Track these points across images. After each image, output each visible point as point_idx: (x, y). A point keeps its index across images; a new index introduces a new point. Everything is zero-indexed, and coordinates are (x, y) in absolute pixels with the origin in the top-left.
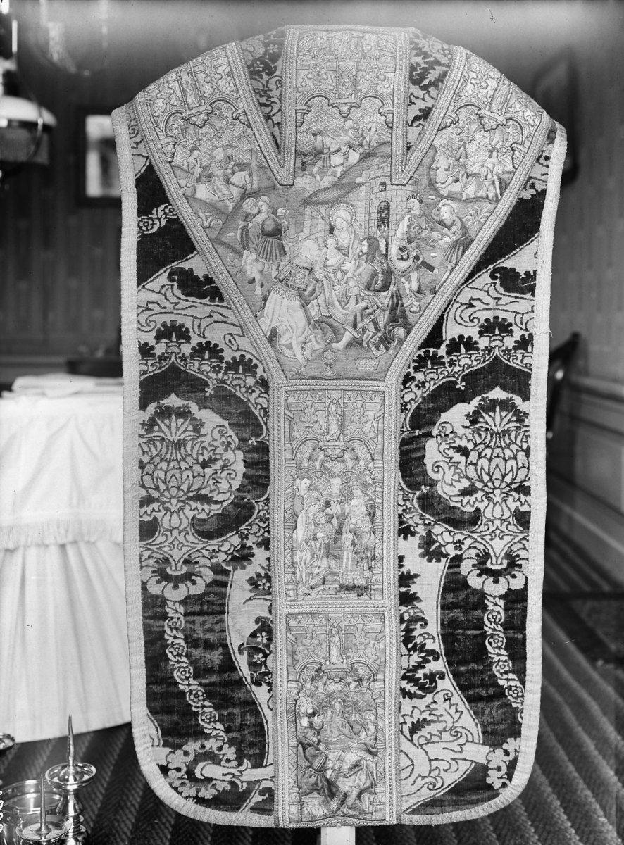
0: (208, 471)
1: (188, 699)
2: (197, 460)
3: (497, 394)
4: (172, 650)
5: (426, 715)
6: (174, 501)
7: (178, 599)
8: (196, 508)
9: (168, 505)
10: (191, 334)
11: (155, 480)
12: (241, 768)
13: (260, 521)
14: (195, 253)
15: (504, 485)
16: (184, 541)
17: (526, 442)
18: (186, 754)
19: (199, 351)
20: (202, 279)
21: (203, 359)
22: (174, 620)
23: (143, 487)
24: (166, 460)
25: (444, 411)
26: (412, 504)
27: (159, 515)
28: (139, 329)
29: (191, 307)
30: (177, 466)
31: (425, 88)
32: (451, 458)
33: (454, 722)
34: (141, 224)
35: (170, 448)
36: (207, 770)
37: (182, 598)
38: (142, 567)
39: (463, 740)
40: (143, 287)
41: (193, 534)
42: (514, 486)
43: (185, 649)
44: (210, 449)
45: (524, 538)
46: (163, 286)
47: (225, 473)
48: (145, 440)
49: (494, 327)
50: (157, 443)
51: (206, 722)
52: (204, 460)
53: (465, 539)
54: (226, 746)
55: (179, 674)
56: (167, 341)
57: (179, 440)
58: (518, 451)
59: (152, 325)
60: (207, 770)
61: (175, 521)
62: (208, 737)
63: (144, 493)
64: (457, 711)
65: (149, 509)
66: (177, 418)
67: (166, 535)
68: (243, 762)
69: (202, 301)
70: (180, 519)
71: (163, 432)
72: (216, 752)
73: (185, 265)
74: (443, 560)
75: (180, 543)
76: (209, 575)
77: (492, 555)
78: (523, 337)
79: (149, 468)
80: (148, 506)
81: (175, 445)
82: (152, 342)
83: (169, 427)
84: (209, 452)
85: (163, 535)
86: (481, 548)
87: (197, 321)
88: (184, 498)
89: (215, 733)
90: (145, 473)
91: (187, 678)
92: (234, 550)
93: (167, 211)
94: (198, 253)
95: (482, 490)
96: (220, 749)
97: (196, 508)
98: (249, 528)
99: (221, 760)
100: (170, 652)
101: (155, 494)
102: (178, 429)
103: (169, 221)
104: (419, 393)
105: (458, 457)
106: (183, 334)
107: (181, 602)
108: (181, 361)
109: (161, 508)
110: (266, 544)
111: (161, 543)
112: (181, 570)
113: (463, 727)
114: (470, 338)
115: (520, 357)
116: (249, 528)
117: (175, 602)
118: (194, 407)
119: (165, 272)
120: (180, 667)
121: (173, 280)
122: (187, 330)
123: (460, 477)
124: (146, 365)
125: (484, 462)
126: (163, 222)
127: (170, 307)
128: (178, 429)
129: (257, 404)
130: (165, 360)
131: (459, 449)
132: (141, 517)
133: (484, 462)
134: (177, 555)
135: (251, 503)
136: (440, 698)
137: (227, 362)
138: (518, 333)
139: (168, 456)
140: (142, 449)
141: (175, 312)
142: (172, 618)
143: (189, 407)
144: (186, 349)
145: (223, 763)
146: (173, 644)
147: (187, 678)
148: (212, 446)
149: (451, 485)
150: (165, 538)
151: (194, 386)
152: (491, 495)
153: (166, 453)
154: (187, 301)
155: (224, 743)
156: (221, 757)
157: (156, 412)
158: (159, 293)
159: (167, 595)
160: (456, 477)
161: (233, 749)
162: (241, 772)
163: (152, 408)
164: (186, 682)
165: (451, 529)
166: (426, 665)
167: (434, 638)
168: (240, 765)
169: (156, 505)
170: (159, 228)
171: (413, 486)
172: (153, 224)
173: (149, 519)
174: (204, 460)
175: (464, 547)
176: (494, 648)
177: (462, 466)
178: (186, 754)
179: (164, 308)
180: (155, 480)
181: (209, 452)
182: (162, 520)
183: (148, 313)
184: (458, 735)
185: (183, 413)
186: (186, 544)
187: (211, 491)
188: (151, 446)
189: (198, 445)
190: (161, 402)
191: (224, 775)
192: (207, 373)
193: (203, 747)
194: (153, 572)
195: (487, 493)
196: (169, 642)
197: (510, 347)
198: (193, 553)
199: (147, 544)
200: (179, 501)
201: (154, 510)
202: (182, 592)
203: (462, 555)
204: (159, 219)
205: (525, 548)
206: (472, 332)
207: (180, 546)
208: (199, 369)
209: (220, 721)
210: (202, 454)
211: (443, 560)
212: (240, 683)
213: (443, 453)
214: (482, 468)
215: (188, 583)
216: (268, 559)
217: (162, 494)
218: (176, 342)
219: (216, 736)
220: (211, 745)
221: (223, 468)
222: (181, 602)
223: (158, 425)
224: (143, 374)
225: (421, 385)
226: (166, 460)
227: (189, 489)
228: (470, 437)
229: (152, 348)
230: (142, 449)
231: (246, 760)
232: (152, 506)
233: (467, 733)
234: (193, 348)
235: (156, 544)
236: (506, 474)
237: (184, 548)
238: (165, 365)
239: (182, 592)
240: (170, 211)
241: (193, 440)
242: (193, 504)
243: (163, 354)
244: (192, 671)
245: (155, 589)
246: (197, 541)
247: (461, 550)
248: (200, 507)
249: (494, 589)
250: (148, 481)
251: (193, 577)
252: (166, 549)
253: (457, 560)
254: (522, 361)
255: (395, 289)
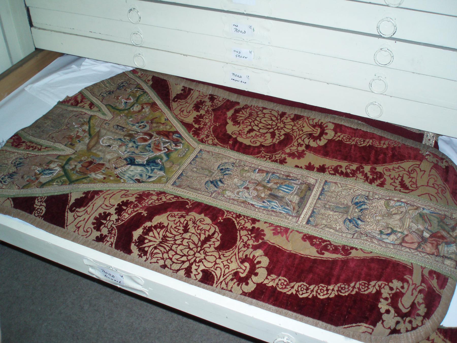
0: (192, 230)
1: (343, 295)
2: (180, 234)
3: (230, 113)
4: (301, 293)
5: (397, 182)
6: (198, 255)
7: (266, 275)
8: (210, 245)
9: (198, 260)
10: (108, 211)
11: (178, 262)
12: (410, 282)
13: (239, 218)
14: (69, 195)
15: (276, 121)
16: (226, 259)
17: (259, 108)
18: (388, 312)
19: (119, 210)
20: (84, 195)
21: (125, 210)
22: (279, 283)
23: (178, 270)
24: (169, 250)
25: (227, 131)
26: (267, 155)
27: (202, 267)
28: (87, 237)
29: (93, 205)
30: (177, 246)
31: (82, 102)
32: (252, 136)
33: (405, 171)
34: (36, 215)
35: (162, 245)
36: (405, 303)
37: (266, 273)
38: (231, 291)
39: (418, 170)
40: (67, 226)
41: (226, 252)
42: (279, 118)
43: (305, 284)
44: (178, 224)
45: (308, 118)
46: (74, 216)
47: (198, 223)
48: (150, 258)
49: (197, 107)
50: (155, 251)
51: (367, 290)
52: (183, 230)
53: (298, 142)
54: (390, 284)
55: (322, 294)
56: (103, 226)
57: (162, 239)
58: (262, 112)
59: (89, 230)
60: (405, 303)
61: (212, 259)
62: (379, 293)
63: (182, 272)
64: (398, 168)
65: (194, 272)
66: (148, 235)
67: (217, 267)
68: (406, 279)
69: (94, 199)
70: (211, 255)
71: (150, 246)
72: (393, 292)
73: (72, 201)
74: (305, 152)
75: (227, 260)
76: (259, 252)
77: (311, 132)
78: (209, 98)
79: (168, 262)
80: (192, 272)
81: (163, 241)
82: (98, 234)
83: (150, 241)
84: (180, 226)
85: (216, 269)
86: (305, 136)
87: (103, 206)
88: (199, 249)
89: (377, 287)
90: (169, 266)
91: (327, 290)
92: (250, 235)
93: (40, 200)
94: (71, 193)
95: (275, 130)
96: (391, 289)
97: (210, 245)
98: (240, 224)
99: (401, 291)
100: (302, 295)
101: (186, 265)
102: (155, 237)
103: (45, 202)
104: (210, 137)
105: (253, 134)
106: (106, 216)
107: (269, 274)
108: (118, 222)
109: (197, 264)
110: (254, 221)
111: (221, 273)
112: (246, 267)
113: (409, 168)
114: (197, 116)
115: (218, 102)
116: (240, 224)
117: (267, 278)
118: (148, 224)
119: (68, 213)
120: (317, 292)
121: (75, 210)
122: (105, 213)
123: (263, 136)
124: (108, 242)
125: (260, 125)
126: (44, 204)
127: (87, 217)
128: (155, 237)
129: (169, 199)
130: (112, 230)
131: (249, 131)
132: (197, 279)
133: (260, 125)
134: (234, 266)
135: (225, 219)
136: (387, 173)
137: (136, 201)
138: (207, 99)
139: (168, 249)
140: (154, 263)
141: (91, 214)
142: (277, 284)
143: (146, 226)
144: (114, 217)
145: (403, 291)
146: (297, 291)
147: (327, 290)
148: (177, 223)
149: (266, 140)
150: (218, 269)
151: (137, 221)
152: (279, 128)
153: (165, 248)
154: (89, 206)
155: (388, 285)
156: (398, 290)
157: (137, 246)
158: (75, 219)
159: (260, 282)
160: (263, 137)
161: (395, 281)
162: (413, 284)
163: (133, 247)
164: (330, 292)
165: (290, 146)
166: (365, 172)
167: (350, 165)
168: (408, 282)
169: (194, 267)
170: (45, 208)
171: (259, 152)
172: (41, 209)
173: (201, 274)
174: (183, 230)
175: (302, 143)
176: (364, 143)
177: (258, 134)
178: (388, 312)
179: (84, 219)
180: (178, 262)
181: (180, 226)
182: (205, 267)
183: (81, 229)
184: (414, 170)
185: (148, 231)
186: (230, 258)
187: (205, 234)
188: (155, 256)
189: (171, 229)
190: (134, 241)
191: (412, 294)
192: (134, 211)
193: (386, 299)
194: (238, 285)
195: (278, 129)
196: (294, 293)
197: (211, 104)
198: (239, 256)
199: (217, 282)
200: (199, 252)
201: (196, 270)
202: (262, 272)
203: (306, 145)
204: (41, 205)
205: (313, 119)
206: (195, 114)
207: (229, 261)
208: (129, 214)
209: (369, 281)
210: (179, 229)
211: (305, 152)
212: (345, 262)
213: (247, 138)
214: (263, 127)
215: (257, 266)
216: (265, 222)
217: (189, 260)
218: (107, 221)
219: (380, 287)
220: (386, 292)
221: (194, 223)
222: (269, 274)
223: (145, 247)
224: (112, 245)
225: (207, 136)
226: (169, 250)
227: (194, 244)
228: (245, 126)
229: (101, 235)
230: (154, 263)
231: (405, 277)
232: (193, 270)
233: (414, 166)
234: (116, 213)
235: (220, 277)
236: (271, 119)
237: (232, 260)
238: (115, 231)
239: (262, 272)
240: (41, 199)
241: (167, 231)
242: (207, 245)
243: (109, 231)
244: (323, 285)
245: (251, 287)
246: (232, 252)
247: (303, 145)
248: (211, 243)
249: (330, 134)
250: (176, 267)
251: (255, 262)
252: (227, 271)
253: (308, 147)
254: (220, 101)
255: (155, 133)
